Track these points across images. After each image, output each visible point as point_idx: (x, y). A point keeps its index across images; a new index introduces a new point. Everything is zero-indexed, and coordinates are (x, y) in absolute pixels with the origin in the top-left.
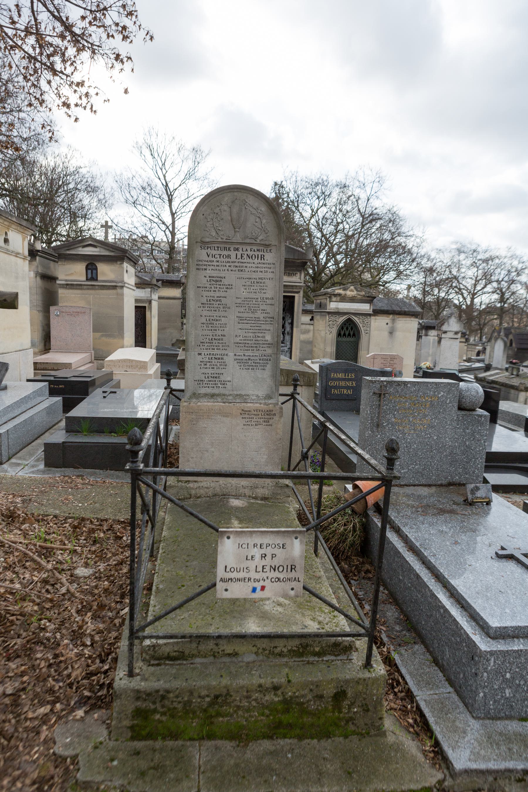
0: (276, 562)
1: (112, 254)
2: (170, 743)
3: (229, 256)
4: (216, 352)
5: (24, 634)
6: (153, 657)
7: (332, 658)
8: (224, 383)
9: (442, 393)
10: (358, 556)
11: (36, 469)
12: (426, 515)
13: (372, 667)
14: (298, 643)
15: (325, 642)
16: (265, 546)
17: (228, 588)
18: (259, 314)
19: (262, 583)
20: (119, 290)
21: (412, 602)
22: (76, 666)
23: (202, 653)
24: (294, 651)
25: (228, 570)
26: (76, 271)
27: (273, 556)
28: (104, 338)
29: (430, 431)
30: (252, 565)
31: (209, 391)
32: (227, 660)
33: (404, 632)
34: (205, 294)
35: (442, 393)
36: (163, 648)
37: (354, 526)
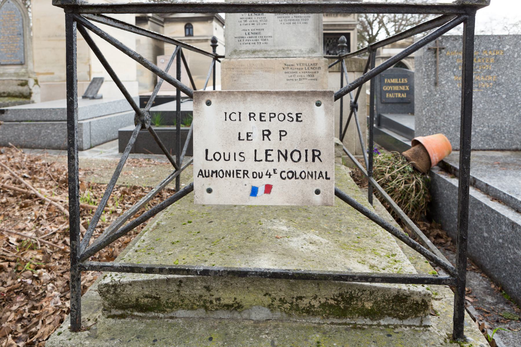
0: (287, 145)
5: (9, 282)
6: (115, 305)
7: (395, 321)
8: (265, 39)
9: (508, 47)
10: (424, 221)
11: (111, 154)
12: (507, 170)
13: (466, 341)
14: (337, 293)
15: (380, 293)
16: (267, 117)
17: (211, 187)
19: (266, 180)
21: (507, 263)
22: (48, 322)
23: (186, 301)
24: (331, 306)
25: (210, 157)
27: (282, 134)
29: (497, 88)
30: (248, 148)
32: (224, 315)
33: (501, 305)
35: (508, 47)
36: (128, 290)
37: (416, 185)
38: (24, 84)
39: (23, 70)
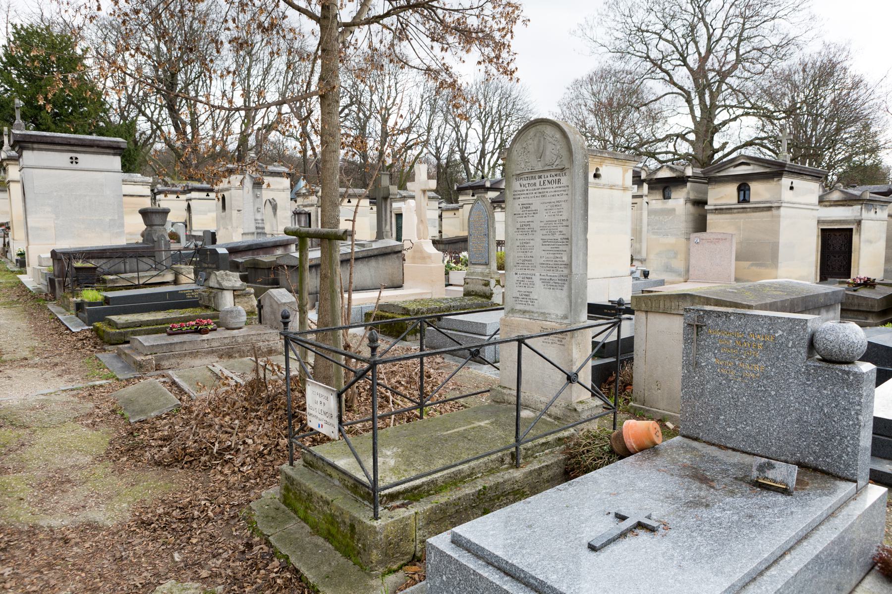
1: (767, 170)
2: (292, 514)
3: (535, 184)
4: (527, 272)
8: (533, 300)
18: (558, 237)
20: (774, 212)
26: (726, 194)
28: (754, 268)
29: (765, 382)
31: (522, 307)
34: (520, 220)
35: (780, 332)
38: (487, 284)
39: (487, 270)
